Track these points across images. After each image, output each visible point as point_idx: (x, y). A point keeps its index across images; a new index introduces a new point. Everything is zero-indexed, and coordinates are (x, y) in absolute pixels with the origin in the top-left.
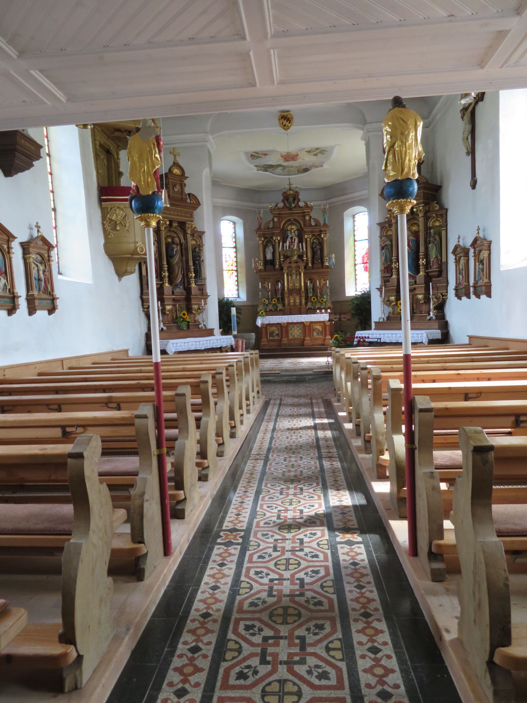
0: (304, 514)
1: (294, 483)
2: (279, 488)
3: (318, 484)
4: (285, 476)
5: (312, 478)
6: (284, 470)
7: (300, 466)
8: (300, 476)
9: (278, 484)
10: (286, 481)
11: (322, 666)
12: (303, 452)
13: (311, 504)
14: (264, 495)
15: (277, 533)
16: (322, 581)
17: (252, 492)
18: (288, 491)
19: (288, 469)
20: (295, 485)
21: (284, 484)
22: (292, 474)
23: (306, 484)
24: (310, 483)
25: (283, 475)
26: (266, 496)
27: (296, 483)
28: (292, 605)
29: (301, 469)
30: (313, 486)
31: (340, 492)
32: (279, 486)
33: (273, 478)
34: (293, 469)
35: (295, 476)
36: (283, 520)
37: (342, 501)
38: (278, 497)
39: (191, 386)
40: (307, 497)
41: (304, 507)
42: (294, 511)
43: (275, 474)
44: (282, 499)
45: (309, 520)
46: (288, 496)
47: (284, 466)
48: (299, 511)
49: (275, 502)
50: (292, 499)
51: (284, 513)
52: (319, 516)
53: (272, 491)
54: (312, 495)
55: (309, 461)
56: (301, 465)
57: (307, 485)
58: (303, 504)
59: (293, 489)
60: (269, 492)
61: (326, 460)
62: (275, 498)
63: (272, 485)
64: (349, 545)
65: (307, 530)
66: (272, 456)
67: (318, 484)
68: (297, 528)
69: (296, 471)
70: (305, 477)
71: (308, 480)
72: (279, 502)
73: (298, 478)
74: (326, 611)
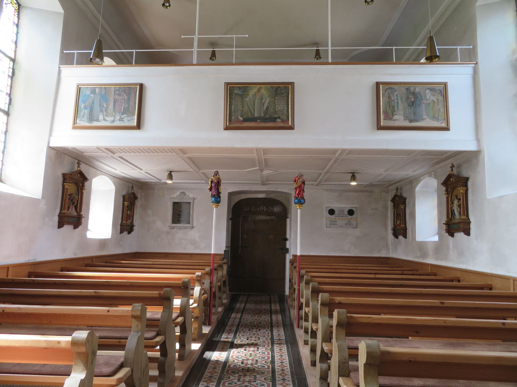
0: (244, 349)
1: (247, 368)
2: (259, 364)
3: (229, 366)
4: (257, 347)
9: (260, 367)
13: (239, 353)
14: (268, 360)
15: (256, 367)
16: (228, 380)
17: (277, 362)
18: (252, 362)
19: (250, 384)
20: (247, 366)
21: (255, 368)
22: (247, 378)
23: (238, 367)
24: (235, 367)
25: (258, 348)
26: (267, 359)
27: (245, 368)
28: (246, 372)
30: (234, 365)
31: (217, 359)
32: (259, 366)
35: (245, 375)
36: (252, 374)
37: (220, 354)
38: (259, 358)
39: (318, 283)
40: (240, 358)
42: (249, 351)
44: (257, 357)
45: (242, 346)
47: (260, 334)
48: (244, 363)
49: (261, 355)
50: (250, 357)
51: (255, 350)
52: (236, 347)
53: (264, 362)
54: (237, 358)
57: (238, 366)
58: (243, 353)
59: (248, 363)
60: (265, 362)
62: (261, 358)
63: (264, 367)
65: (244, 343)
67: (229, 366)
68: (244, 369)
71: (236, 370)
72: (258, 355)
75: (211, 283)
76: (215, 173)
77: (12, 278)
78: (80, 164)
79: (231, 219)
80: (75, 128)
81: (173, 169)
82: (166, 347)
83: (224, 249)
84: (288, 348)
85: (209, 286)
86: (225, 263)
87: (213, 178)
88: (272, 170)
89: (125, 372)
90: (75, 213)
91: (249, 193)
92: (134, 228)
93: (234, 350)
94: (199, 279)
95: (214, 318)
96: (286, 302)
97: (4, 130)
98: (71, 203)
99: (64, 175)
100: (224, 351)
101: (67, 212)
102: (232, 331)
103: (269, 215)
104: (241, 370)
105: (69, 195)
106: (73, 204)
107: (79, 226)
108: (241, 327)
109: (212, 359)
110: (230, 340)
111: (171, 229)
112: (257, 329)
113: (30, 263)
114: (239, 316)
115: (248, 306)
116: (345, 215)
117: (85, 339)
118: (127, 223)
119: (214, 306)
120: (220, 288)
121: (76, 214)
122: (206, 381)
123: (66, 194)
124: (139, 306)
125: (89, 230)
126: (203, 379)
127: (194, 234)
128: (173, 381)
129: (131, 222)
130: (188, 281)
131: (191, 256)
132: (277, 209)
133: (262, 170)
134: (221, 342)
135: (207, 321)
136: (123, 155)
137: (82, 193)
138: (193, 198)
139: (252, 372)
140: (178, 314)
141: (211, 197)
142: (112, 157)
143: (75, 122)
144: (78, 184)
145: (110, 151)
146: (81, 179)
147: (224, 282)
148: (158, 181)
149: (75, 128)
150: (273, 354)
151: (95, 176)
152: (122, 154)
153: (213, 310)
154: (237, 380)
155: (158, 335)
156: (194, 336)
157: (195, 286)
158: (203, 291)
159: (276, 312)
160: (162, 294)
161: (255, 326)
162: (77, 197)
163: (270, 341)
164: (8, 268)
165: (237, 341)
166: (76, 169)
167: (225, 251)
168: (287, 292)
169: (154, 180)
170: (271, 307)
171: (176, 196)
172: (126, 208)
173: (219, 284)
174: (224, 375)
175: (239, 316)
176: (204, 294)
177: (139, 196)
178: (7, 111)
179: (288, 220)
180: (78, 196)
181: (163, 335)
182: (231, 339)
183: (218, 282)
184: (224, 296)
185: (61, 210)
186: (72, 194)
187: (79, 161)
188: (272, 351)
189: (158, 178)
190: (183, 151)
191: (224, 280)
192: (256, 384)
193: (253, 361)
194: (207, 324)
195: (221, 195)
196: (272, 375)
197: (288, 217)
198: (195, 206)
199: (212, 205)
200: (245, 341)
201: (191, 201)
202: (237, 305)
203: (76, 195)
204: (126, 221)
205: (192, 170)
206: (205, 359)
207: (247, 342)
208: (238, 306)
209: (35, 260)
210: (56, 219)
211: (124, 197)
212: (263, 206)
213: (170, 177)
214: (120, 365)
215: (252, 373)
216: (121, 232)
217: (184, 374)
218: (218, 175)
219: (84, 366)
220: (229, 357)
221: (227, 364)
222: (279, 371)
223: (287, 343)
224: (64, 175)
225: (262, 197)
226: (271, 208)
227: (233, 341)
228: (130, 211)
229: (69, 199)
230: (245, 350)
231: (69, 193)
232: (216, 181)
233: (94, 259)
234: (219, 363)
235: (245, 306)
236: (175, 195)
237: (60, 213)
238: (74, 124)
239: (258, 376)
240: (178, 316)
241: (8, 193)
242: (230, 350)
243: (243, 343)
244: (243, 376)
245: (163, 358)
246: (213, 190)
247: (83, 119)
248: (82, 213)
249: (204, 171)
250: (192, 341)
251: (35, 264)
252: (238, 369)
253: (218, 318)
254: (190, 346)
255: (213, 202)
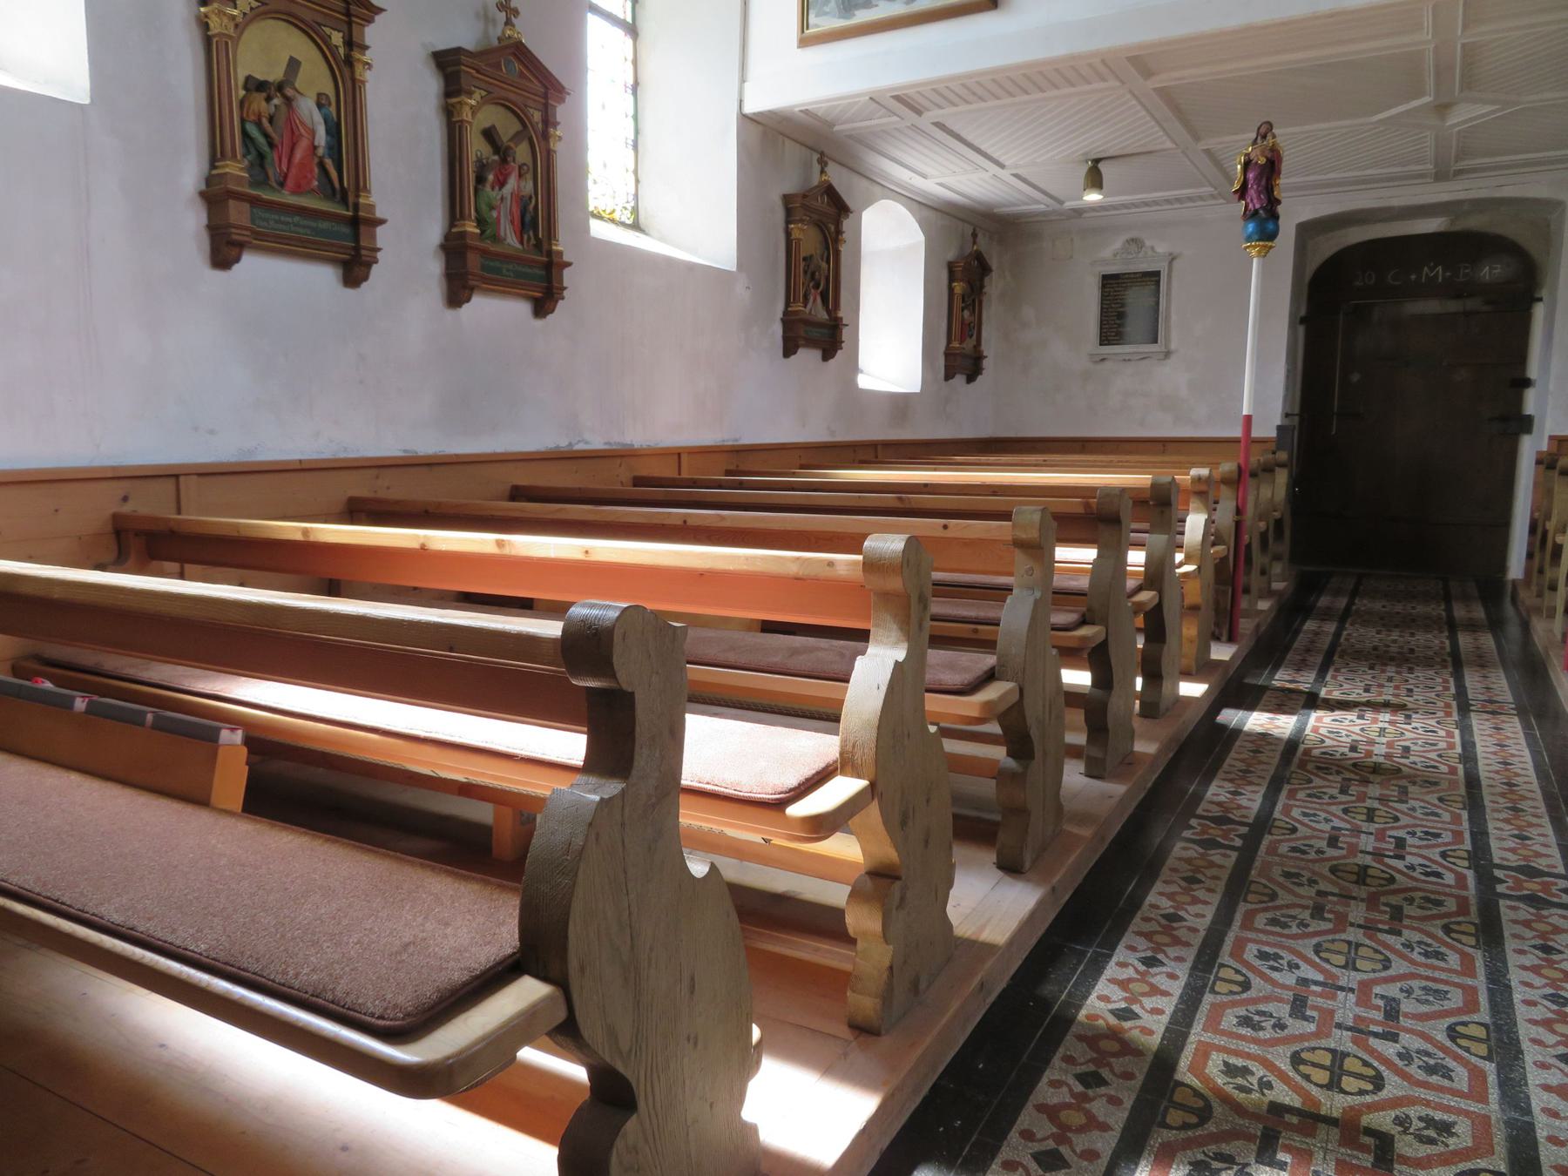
1: (1372, 765)
5: (1319, 768)
6: (1403, 807)
7: (1346, 811)
8: (1350, 780)
10: (1396, 772)
11: (1234, 1088)
12: (1317, 867)
15: (1399, 871)
18: (1388, 750)
20: (1369, 760)
22: (1374, 790)
23: (1338, 756)
25: (1408, 717)
27: (1366, 764)
29: (1343, 798)
33: (1436, 784)
34: (1369, 803)
36: (1392, 782)
41: (1283, 1027)
43: (1433, 799)
46: (1362, 983)
47: (1404, 820)
55: (1306, 820)
56: (1340, 813)
57: (1338, 754)
61: (1244, 812)
64: (1202, 848)
66: (1461, 879)
69: (1362, 797)
70: (1338, 773)
71: (1332, 764)
73: (1356, 774)
74: (1220, 1049)
75: (1239, 511)
76: (1259, 129)
77: (690, 477)
78: (826, 164)
79: (1303, 321)
80: (805, 42)
81: (1103, 151)
82: (1110, 661)
83: (1278, 422)
84: (1527, 727)
85: (1231, 520)
86: (1282, 465)
87: (1250, 149)
88: (1493, 102)
89: (1002, 691)
90: (823, 315)
91: (1380, 221)
92: (985, 363)
93: (1320, 713)
94: (1203, 488)
95: (1246, 626)
96: (1508, 599)
97: (631, 81)
98: (811, 285)
99: (787, 199)
100: (1285, 713)
101: (801, 308)
102: (1307, 665)
103: (1458, 296)
104: (1351, 768)
105: (805, 259)
106: (817, 286)
107: (836, 352)
108: (1341, 657)
109: (1246, 728)
110: (1304, 687)
111: (1096, 362)
112: (1399, 666)
113: (727, 446)
114: (1331, 627)
115: (1362, 604)
116: (1443, 822)
117: (901, 555)
118: (964, 349)
119: (1247, 591)
120: (1264, 537)
121: (826, 317)
122: (1148, 936)
123: (797, 258)
124: (1036, 511)
125: (862, 372)
126: (1220, 774)
127: (1172, 376)
128: (1130, 764)
129: (975, 347)
130: (1170, 483)
131: (1164, 446)
132: (1491, 271)
133: (1442, 108)
134: (1272, 690)
135: (1224, 625)
136: (945, 114)
137: (837, 253)
138: (1170, 254)
139: (1392, 776)
140: (1140, 582)
141: (1243, 222)
142: (914, 127)
143: (804, 24)
144: (824, 224)
145: (907, 101)
146: (832, 211)
147: (1279, 524)
148: (1054, 205)
149: (805, 42)
150: (1467, 737)
151: (869, 202)
152: (941, 112)
153: (1244, 603)
154: (1337, 791)
155: (1083, 622)
156: (1184, 662)
157: (1187, 512)
158: (1212, 535)
159: (1472, 627)
160: (1094, 506)
161: (1392, 659)
162: (824, 265)
163: (1455, 702)
164: (679, 454)
165: (1329, 692)
166: (816, 180)
167: (1279, 428)
168: (1516, 567)
169: (1041, 205)
170: (1449, 610)
171: (1111, 256)
172: (957, 303)
173: (1262, 525)
174: (1293, 772)
175: (1331, 627)
176: (1214, 544)
177: (994, 264)
178: (631, 22)
179: (1539, 311)
180: (828, 262)
181: (1101, 625)
182: (1309, 686)
183: (1260, 520)
184: (1277, 568)
185: (787, 304)
186: (811, 256)
187: (822, 154)
188: (1466, 730)
189: (1052, 193)
190: (1141, 62)
191: (1279, 517)
192: (1297, 967)
193: (1390, 748)
194: (1224, 638)
195: (1280, 209)
196: (1468, 793)
197: (1540, 300)
198: (1175, 284)
199: (1248, 247)
200: (1357, 694)
201: (1162, 266)
202: (1322, 599)
203: (822, 260)
204: (962, 342)
205: (1169, 145)
206: (1223, 727)
207: (1365, 697)
208: (1324, 601)
209: (736, 440)
210: (778, 329)
211: (951, 267)
212: (1432, 264)
213: (1095, 179)
214: (986, 672)
215: (1390, 780)
216: (948, 376)
217: (1160, 751)
218: (1269, 137)
219: (901, 629)
220: (1305, 730)
221: (1298, 746)
222: (1494, 784)
223: (1522, 712)
224: (787, 199)
225: (1431, 231)
226: (1467, 268)
227: (1314, 690)
228: (969, 310)
229: (805, 272)
230: (1361, 717)
231: (805, 255)
232: (1262, 161)
233: (879, 447)
234: (1270, 740)
235: (1351, 603)
236: (1107, 253)
237: (786, 313)
238: (803, 32)
239: (1411, 789)
240: (1139, 589)
241: (658, 254)
242: (1306, 711)
243: (1351, 698)
244: (1356, 783)
245: (1099, 692)
246: (1252, 192)
247: (827, 9)
248: (840, 314)
249: (1210, 143)
250: (1181, 676)
251: (737, 451)
252: (1337, 762)
253: (1258, 626)
254: (1176, 687)
255: (1249, 239)
